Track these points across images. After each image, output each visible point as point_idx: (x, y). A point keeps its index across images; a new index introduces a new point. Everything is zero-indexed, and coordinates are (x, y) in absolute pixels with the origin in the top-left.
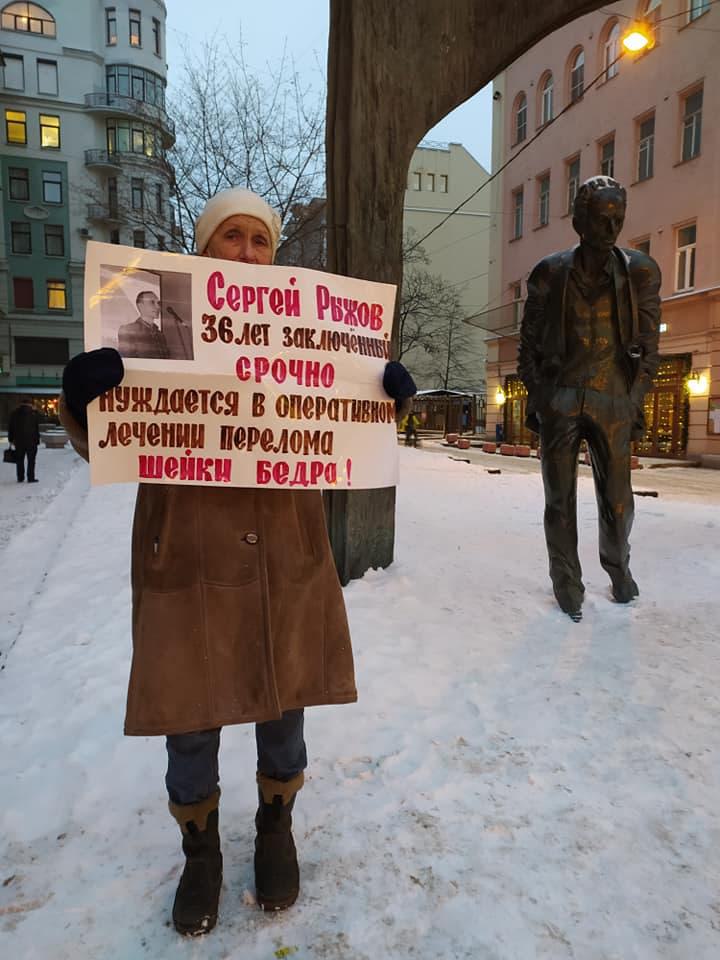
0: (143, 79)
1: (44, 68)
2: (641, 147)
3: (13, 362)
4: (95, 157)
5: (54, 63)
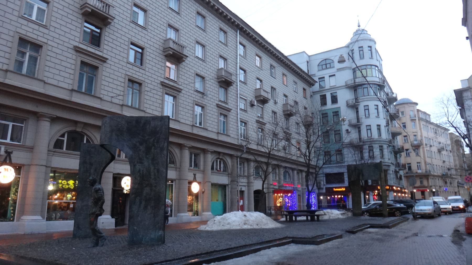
0: (366, 69)
1: (331, 78)
3: (325, 184)
4: (350, 102)
5: (334, 75)
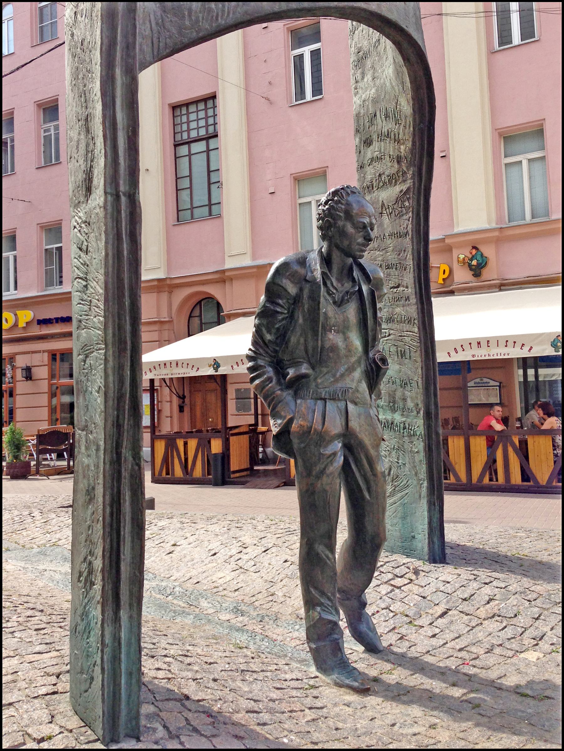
2: (45, 131)
